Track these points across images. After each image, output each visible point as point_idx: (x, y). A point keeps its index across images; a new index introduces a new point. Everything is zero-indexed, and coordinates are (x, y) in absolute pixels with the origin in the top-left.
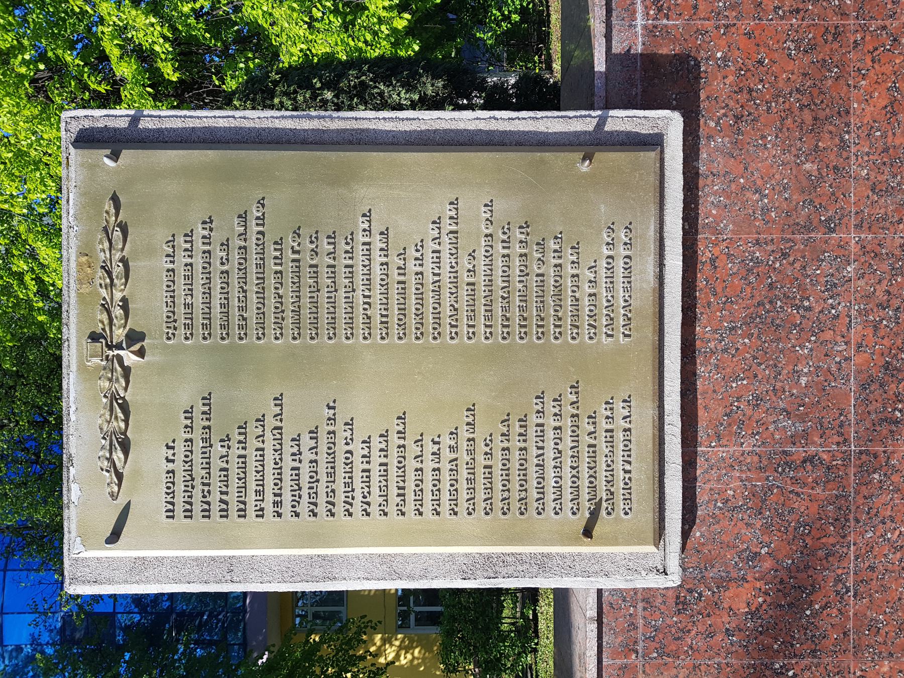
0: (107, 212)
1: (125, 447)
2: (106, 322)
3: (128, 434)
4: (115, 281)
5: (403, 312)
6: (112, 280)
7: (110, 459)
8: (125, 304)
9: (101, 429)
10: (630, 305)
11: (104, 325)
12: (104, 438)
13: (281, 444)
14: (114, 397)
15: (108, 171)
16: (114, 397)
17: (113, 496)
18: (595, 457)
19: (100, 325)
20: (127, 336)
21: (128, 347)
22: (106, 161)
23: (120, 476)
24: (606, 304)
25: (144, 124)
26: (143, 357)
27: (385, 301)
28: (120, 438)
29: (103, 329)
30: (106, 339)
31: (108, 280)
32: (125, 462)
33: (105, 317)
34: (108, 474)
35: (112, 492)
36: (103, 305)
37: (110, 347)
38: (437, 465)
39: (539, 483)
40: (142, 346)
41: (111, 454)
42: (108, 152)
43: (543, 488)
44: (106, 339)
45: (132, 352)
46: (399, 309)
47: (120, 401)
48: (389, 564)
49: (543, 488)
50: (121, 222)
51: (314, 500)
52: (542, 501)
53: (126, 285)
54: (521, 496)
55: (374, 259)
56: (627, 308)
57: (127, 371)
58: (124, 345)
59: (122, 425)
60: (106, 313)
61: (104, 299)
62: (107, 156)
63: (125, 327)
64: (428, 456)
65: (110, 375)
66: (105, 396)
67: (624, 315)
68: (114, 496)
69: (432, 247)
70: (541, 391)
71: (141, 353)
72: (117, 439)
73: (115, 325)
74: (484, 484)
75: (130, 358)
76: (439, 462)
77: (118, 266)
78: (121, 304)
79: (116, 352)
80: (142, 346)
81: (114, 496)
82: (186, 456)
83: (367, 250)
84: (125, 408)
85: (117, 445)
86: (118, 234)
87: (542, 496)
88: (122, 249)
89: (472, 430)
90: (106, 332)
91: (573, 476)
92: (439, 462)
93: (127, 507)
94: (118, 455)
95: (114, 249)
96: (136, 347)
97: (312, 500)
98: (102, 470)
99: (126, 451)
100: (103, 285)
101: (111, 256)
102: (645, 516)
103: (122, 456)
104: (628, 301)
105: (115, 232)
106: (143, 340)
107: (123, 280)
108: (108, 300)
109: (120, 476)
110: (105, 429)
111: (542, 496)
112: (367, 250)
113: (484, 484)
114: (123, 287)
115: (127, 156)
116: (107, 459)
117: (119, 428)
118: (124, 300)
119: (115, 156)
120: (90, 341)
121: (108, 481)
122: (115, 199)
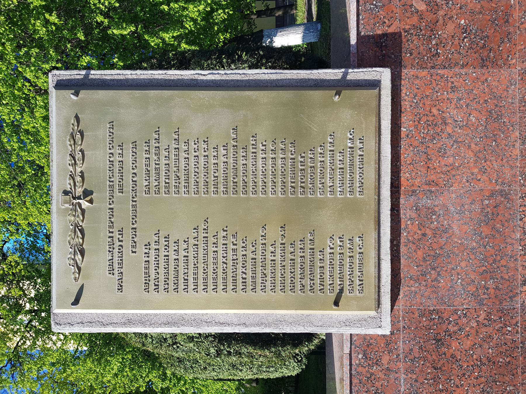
0: (73, 125)
1: (82, 253)
2: (72, 184)
4: (77, 162)
6: (75, 161)
11: (71, 186)
12: (71, 248)
14: (76, 226)
19: (69, 186)
20: (83, 192)
21: (84, 198)
22: (72, 96)
23: (79, 269)
26: (92, 203)
29: (71, 189)
31: (73, 162)
32: (82, 261)
33: (72, 182)
34: (73, 268)
35: (75, 277)
36: (71, 175)
37: (74, 198)
41: (75, 257)
42: (73, 91)
44: (72, 194)
47: (80, 228)
50: (80, 130)
57: (83, 211)
58: (82, 197)
59: (81, 241)
60: (72, 179)
61: (71, 172)
62: (72, 94)
65: (74, 213)
66: (72, 225)
71: (91, 201)
72: (78, 248)
73: (77, 186)
75: (85, 204)
77: (79, 154)
78: (80, 174)
79: (78, 201)
81: (76, 279)
84: (82, 231)
85: (78, 252)
86: (78, 136)
88: (81, 145)
93: (82, 286)
94: (79, 257)
95: (77, 144)
96: (88, 198)
98: (70, 265)
99: (83, 255)
103: (80, 257)
105: (77, 136)
106: (92, 194)
107: (81, 162)
108: (73, 173)
109: (79, 269)
113: (184, 266)
114: (81, 165)
115: (83, 93)
116: (72, 259)
117: (79, 242)
118: (82, 172)
119: (77, 94)
121: (73, 271)
122: (77, 118)
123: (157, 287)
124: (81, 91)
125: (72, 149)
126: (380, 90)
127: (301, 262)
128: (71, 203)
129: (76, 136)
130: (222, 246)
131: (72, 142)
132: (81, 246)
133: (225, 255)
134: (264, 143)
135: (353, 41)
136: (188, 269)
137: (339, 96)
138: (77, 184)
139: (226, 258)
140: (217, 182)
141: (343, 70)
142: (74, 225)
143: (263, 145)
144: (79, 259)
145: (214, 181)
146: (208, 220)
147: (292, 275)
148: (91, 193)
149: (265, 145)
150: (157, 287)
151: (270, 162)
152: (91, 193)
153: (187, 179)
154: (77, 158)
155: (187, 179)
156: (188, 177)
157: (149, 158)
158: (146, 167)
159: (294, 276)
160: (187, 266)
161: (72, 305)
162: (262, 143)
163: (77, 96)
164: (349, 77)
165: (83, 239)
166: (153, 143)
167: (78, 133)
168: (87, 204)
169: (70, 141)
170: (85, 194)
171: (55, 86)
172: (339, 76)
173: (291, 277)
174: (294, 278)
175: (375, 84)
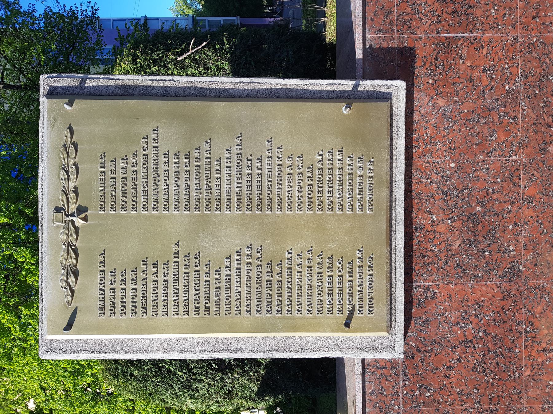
0: (66, 136)
2: (65, 200)
3: (78, 267)
4: (71, 176)
5: (240, 201)
6: (68, 176)
7: (66, 281)
8: (76, 191)
9: (62, 263)
10: (342, 197)
11: (63, 202)
12: (63, 269)
13: (178, 271)
14: (69, 245)
15: (67, 111)
16: (69, 245)
17: (68, 303)
18: (301, 279)
19: (62, 203)
20: (77, 209)
21: (78, 215)
22: (66, 106)
23: (72, 292)
24: (338, 196)
25: (89, 83)
26: (87, 221)
27: (145, 177)
28: (73, 269)
29: (64, 205)
30: (64, 210)
31: (66, 176)
32: (76, 283)
33: (64, 198)
34: (65, 290)
35: (68, 301)
36: (63, 191)
37: (67, 215)
38: (134, 287)
39: (350, 290)
40: (86, 215)
41: (67, 278)
42: (67, 101)
43: (352, 293)
44: (64, 210)
45: (80, 218)
46: (238, 199)
47: (73, 247)
48: (182, 346)
49: (352, 293)
51: (145, 307)
52: (260, 306)
53: (76, 179)
54: (248, 303)
55: (213, 168)
56: (341, 199)
57: (77, 230)
58: (76, 214)
59: (74, 261)
60: (65, 195)
61: (64, 187)
62: (66, 104)
63: (76, 203)
64: (129, 282)
65: (67, 232)
66: (64, 244)
67: (339, 203)
68: (69, 303)
69: (288, 171)
70: (310, 246)
71: (85, 219)
72: (71, 269)
73: (70, 203)
74: (246, 297)
75: (79, 222)
76: (136, 285)
77: (72, 168)
78: (74, 190)
79: (71, 218)
80: (86, 215)
82: (101, 280)
83: (156, 150)
84: (76, 251)
86: (72, 149)
87: (260, 303)
88: (75, 158)
89: (321, 267)
90: (65, 207)
91: (319, 291)
92: (136, 285)
94: (72, 279)
95: (70, 158)
96: (83, 216)
97: (143, 306)
98: (62, 288)
99: (76, 277)
100: (63, 179)
101: (68, 162)
102: (382, 309)
103: (74, 279)
104: (341, 195)
106: (87, 211)
107: (75, 176)
108: (67, 188)
109: (72, 292)
110: (64, 263)
111: (260, 303)
112: (156, 150)
113: (246, 297)
114: (75, 180)
116: (65, 281)
117: (73, 264)
118: (75, 187)
119: (71, 104)
120: (55, 211)
122: (70, 128)
123: (270, 303)
124: (76, 101)
125: (65, 163)
126: (391, 103)
127: (369, 281)
128: (64, 222)
129: (69, 149)
130: (287, 271)
131: (66, 155)
132: (74, 266)
133: (290, 280)
134: (321, 153)
135: (359, 55)
136: (251, 300)
137: (350, 108)
138: (70, 200)
139: (290, 283)
140: (157, 192)
141: (354, 82)
142: (67, 244)
143: (320, 155)
144: (72, 281)
145: (176, 191)
146: (373, 256)
147: (320, 288)
148: (86, 209)
149: (322, 155)
150: (270, 303)
151: (337, 172)
152: (86, 209)
153: (219, 194)
154: (70, 173)
155: (219, 194)
156: (220, 193)
157: (168, 171)
158: (289, 184)
159: (321, 290)
160: (250, 297)
161: (64, 330)
162: (318, 153)
163: (71, 106)
164: (360, 89)
165: (77, 259)
166: (235, 150)
167: (71, 146)
168: (82, 222)
169: (63, 155)
170: (80, 211)
171: (48, 94)
172: (350, 88)
173: (319, 291)
174: (322, 291)
175: (387, 97)
